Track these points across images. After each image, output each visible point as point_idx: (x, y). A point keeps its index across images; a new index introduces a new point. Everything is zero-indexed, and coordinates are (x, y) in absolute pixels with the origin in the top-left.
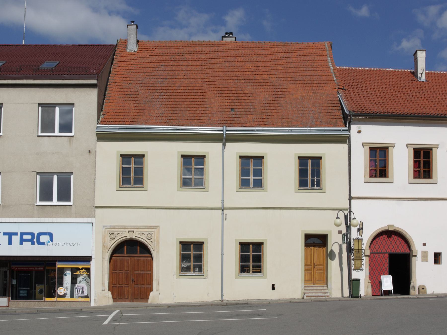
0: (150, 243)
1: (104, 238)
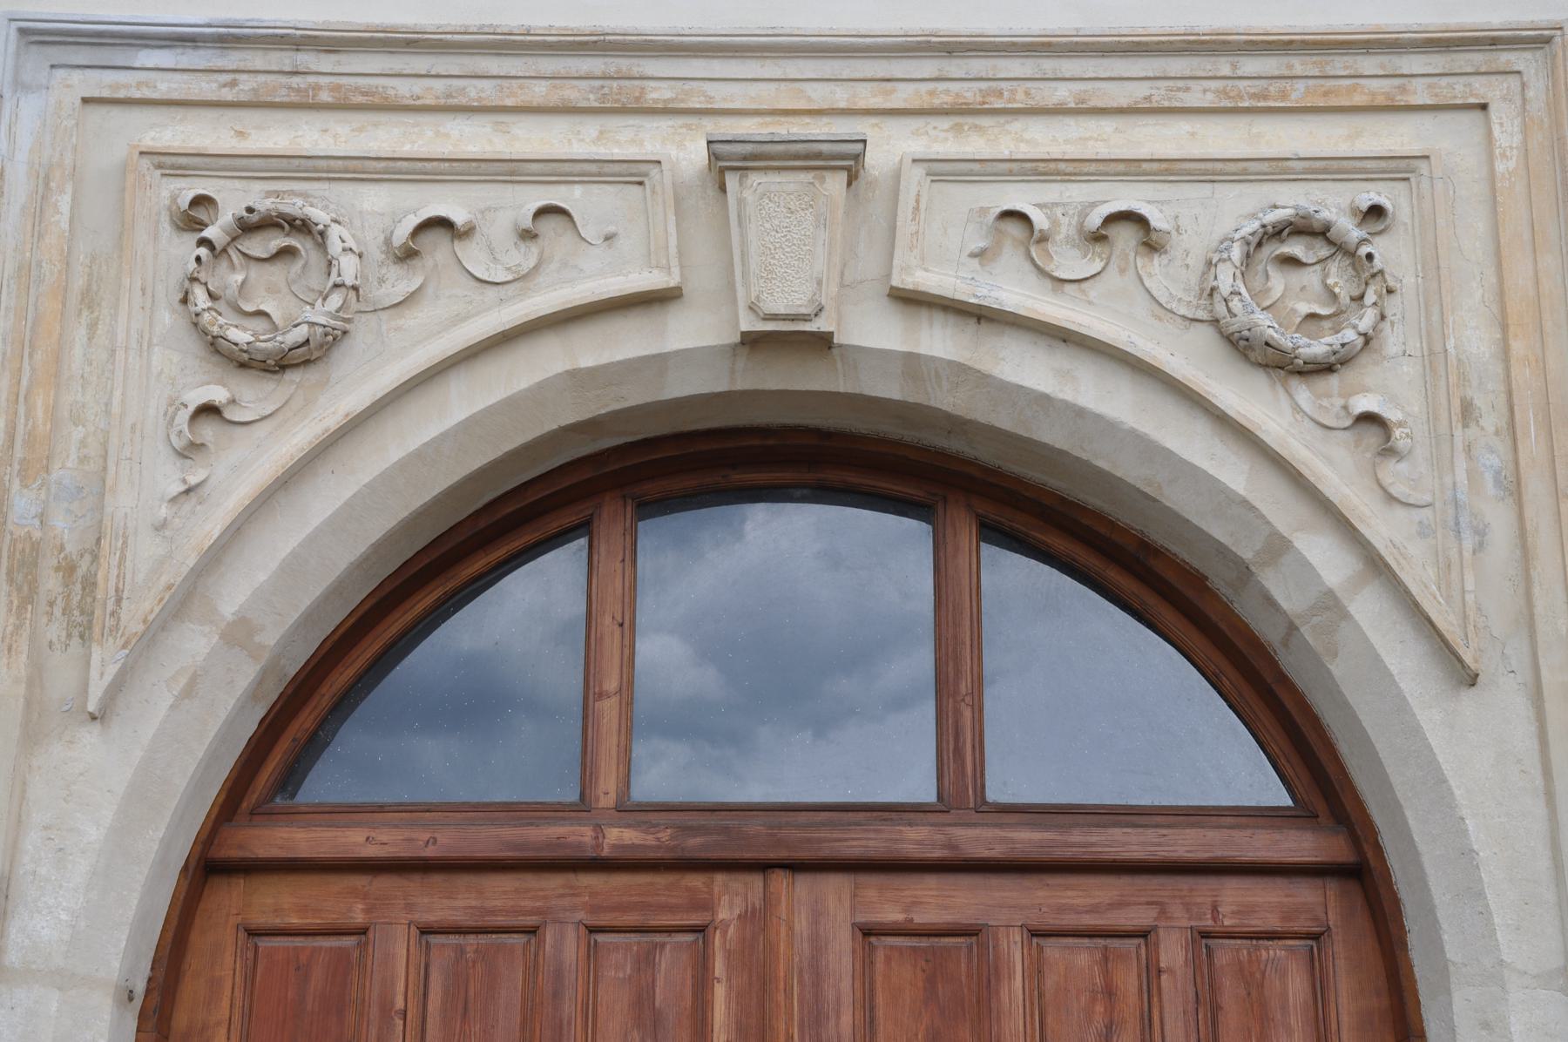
0: (1336, 469)
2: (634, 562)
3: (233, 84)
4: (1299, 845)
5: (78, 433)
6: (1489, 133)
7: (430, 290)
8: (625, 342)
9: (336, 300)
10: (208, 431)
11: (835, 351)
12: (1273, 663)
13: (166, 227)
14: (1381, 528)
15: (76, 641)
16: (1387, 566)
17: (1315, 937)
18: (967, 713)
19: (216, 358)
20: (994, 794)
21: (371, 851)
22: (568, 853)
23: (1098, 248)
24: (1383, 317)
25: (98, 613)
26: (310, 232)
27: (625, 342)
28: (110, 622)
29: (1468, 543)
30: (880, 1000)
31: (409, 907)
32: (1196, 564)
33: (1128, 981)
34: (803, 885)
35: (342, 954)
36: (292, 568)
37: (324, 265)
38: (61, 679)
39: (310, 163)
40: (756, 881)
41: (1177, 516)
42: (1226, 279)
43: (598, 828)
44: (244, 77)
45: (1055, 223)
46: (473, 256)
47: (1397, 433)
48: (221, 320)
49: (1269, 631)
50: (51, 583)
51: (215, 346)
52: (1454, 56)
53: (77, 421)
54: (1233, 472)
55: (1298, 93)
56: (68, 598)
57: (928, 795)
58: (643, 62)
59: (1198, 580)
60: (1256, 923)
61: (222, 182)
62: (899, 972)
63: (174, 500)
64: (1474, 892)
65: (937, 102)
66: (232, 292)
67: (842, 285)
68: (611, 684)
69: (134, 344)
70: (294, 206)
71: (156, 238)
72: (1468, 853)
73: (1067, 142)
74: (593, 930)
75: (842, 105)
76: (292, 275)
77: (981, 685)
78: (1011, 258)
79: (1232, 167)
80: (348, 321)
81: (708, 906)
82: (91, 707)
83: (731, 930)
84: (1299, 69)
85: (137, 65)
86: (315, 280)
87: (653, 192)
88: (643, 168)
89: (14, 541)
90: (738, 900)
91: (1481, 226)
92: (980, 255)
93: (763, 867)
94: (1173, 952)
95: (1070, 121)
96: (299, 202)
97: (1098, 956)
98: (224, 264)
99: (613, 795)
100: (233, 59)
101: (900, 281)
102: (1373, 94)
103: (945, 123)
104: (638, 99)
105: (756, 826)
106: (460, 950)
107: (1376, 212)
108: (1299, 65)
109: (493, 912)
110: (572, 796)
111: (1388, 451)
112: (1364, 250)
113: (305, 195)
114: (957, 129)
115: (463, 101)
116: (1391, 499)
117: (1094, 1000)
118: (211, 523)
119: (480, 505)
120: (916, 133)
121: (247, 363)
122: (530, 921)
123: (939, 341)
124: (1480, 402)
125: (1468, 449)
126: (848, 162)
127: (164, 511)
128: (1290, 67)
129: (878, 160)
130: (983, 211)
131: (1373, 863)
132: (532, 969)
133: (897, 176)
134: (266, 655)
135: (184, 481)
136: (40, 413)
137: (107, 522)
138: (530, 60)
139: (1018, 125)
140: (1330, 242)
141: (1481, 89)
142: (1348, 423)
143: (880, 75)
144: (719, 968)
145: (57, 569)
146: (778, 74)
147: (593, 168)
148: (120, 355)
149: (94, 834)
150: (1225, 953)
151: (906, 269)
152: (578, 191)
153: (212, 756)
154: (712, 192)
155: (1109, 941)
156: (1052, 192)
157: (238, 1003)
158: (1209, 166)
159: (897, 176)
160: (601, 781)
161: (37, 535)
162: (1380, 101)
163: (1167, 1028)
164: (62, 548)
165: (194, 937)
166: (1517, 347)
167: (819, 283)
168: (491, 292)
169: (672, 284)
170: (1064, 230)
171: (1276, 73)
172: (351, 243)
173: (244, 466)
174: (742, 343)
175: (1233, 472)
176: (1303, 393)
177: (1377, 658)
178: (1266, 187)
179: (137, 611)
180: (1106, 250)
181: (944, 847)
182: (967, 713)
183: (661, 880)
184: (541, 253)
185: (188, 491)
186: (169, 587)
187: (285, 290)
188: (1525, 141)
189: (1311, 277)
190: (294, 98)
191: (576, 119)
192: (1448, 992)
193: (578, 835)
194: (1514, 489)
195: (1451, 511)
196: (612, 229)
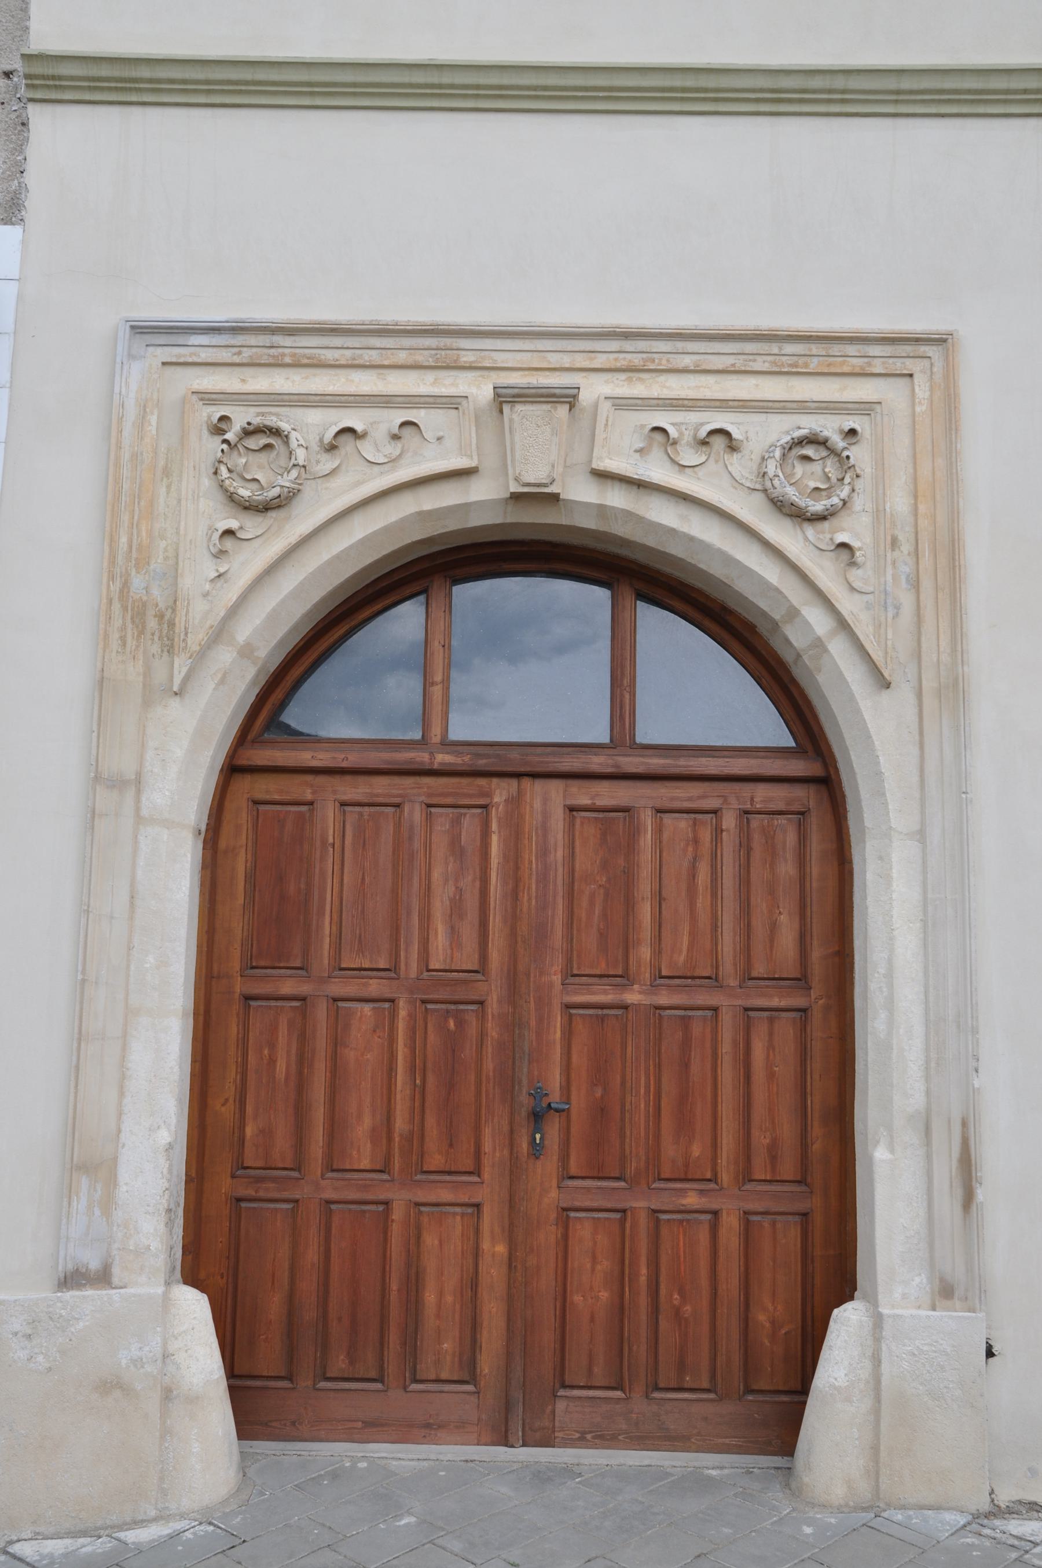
0: (825, 573)
1: (127, 504)
2: (450, 612)
3: (239, 353)
4: (797, 767)
5: (163, 544)
6: (913, 390)
7: (343, 467)
8: (448, 496)
9: (294, 473)
10: (229, 543)
11: (561, 503)
12: (788, 672)
13: (205, 433)
14: (847, 604)
15: (166, 653)
16: (849, 625)
17: (802, 813)
18: (627, 696)
19: (232, 504)
20: (638, 740)
21: (315, 763)
22: (416, 766)
23: (704, 449)
24: (853, 490)
25: (176, 639)
26: (280, 435)
27: (448, 496)
28: (182, 645)
29: (890, 615)
30: (577, 843)
31: (335, 792)
32: (750, 619)
33: (706, 836)
34: (539, 785)
35: (301, 815)
36: (273, 617)
37: (288, 453)
38: (160, 675)
39: (280, 397)
40: (514, 782)
41: (741, 595)
42: (771, 468)
43: (431, 754)
44: (245, 349)
45: (681, 434)
46: (367, 449)
47: (858, 554)
48: (235, 484)
49: (788, 657)
50: (152, 624)
51: (232, 498)
52: (897, 347)
53: (162, 537)
54: (771, 572)
55: (814, 364)
56: (161, 631)
57: (604, 738)
58: (458, 340)
59: (752, 628)
60: (773, 807)
61: (234, 408)
62: (588, 830)
63: (212, 581)
64: (880, 793)
65: (618, 365)
66: (240, 468)
67: (565, 466)
68: (438, 678)
69: (190, 497)
70: (272, 421)
71: (200, 439)
72: (879, 774)
73: (689, 388)
74: (429, 806)
75: (567, 366)
76: (271, 459)
77: (635, 681)
78: (657, 453)
79: (777, 405)
80: (300, 484)
81: (489, 794)
82: (175, 689)
83: (501, 807)
84: (814, 351)
85: (190, 343)
86: (283, 462)
87: (464, 413)
88: (459, 400)
89: (134, 602)
90: (505, 793)
91: (907, 441)
92: (640, 451)
93: (518, 775)
94: (729, 821)
95: (691, 376)
96: (274, 419)
97: (691, 823)
98: (236, 453)
99: (439, 737)
100: (239, 340)
101: (600, 463)
102: (853, 366)
103: (623, 376)
104: (455, 361)
105: (514, 754)
106: (361, 814)
107: (852, 432)
108: (815, 348)
109: (377, 795)
110: (417, 735)
111: (852, 564)
112: (845, 453)
113: (277, 415)
114: (629, 380)
115: (361, 362)
116: (852, 589)
117: (687, 845)
118: (232, 593)
119: (369, 581)
120: (607, 382)
121: (248, 507)
122: (397, 800)
123: (617, 498)
124: (901, 537)
125: (894, 563)
126: (569, 398)
127: (207, 587)
128: (810, 350)
129: (586, 397)
130: (642, 426)
131: (833, 777)
132: (398, 825)
133: (596, 406)
134: (260, 664)
135: (217, 571)
136: (144, 534)
137: (179, 592)
138: (397, 339)
139: (662, 378)
140: (828, 448)
141: (910, 365)
142: (833, 548)
143: (588, 349)
144: (494, 826)
145: (155, 616)
146: (532, 348)
147: (431, 400)
148: (183, 502)
149: (179, 753)
150: (756, 821)
151: (600, 458)
152: (423, 412)
153: (234, 714)
154: (495, 413)
155: (697, 816)
156: (680, 417)
157: (250, 837)
158: (765, 404)
159: (596, 406)
160: (433, 729)
161: (145, 598)
162: (857, 370)
163: (724, 859)
164: (157, 605)
165: (227, 804)
166: (922, 508)
167: (553, 466)
168: (376, 468)
169: (474, 465)
170: (686, 437)
171: (803, 353)
172: (302, 442)
173: (248, 563)
174: (511, 498)
175: (771, 572)
176: (810, 531)
177: (841, 673)
178: (795, 417)
179: (196, 639)
180: (709, 450)
181: (612, 766)
182: (627, 696)
183: (465, 781)
184: (403, 447)
185: (219, 576)
186: (212, 627)
187: (267, 466)
188: (931, 396)
189: (816, 467)
190: (271, 361)
191: (423, 371)
192: (864, 842)
193: (421, 757)
194: (916, 585)
195: (883, 596)
196: (441, 434)
